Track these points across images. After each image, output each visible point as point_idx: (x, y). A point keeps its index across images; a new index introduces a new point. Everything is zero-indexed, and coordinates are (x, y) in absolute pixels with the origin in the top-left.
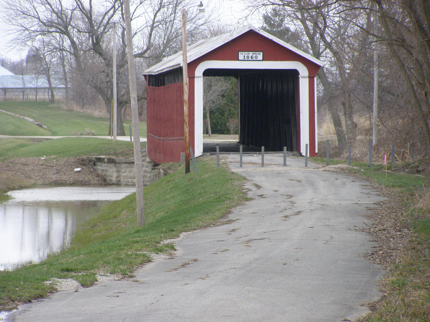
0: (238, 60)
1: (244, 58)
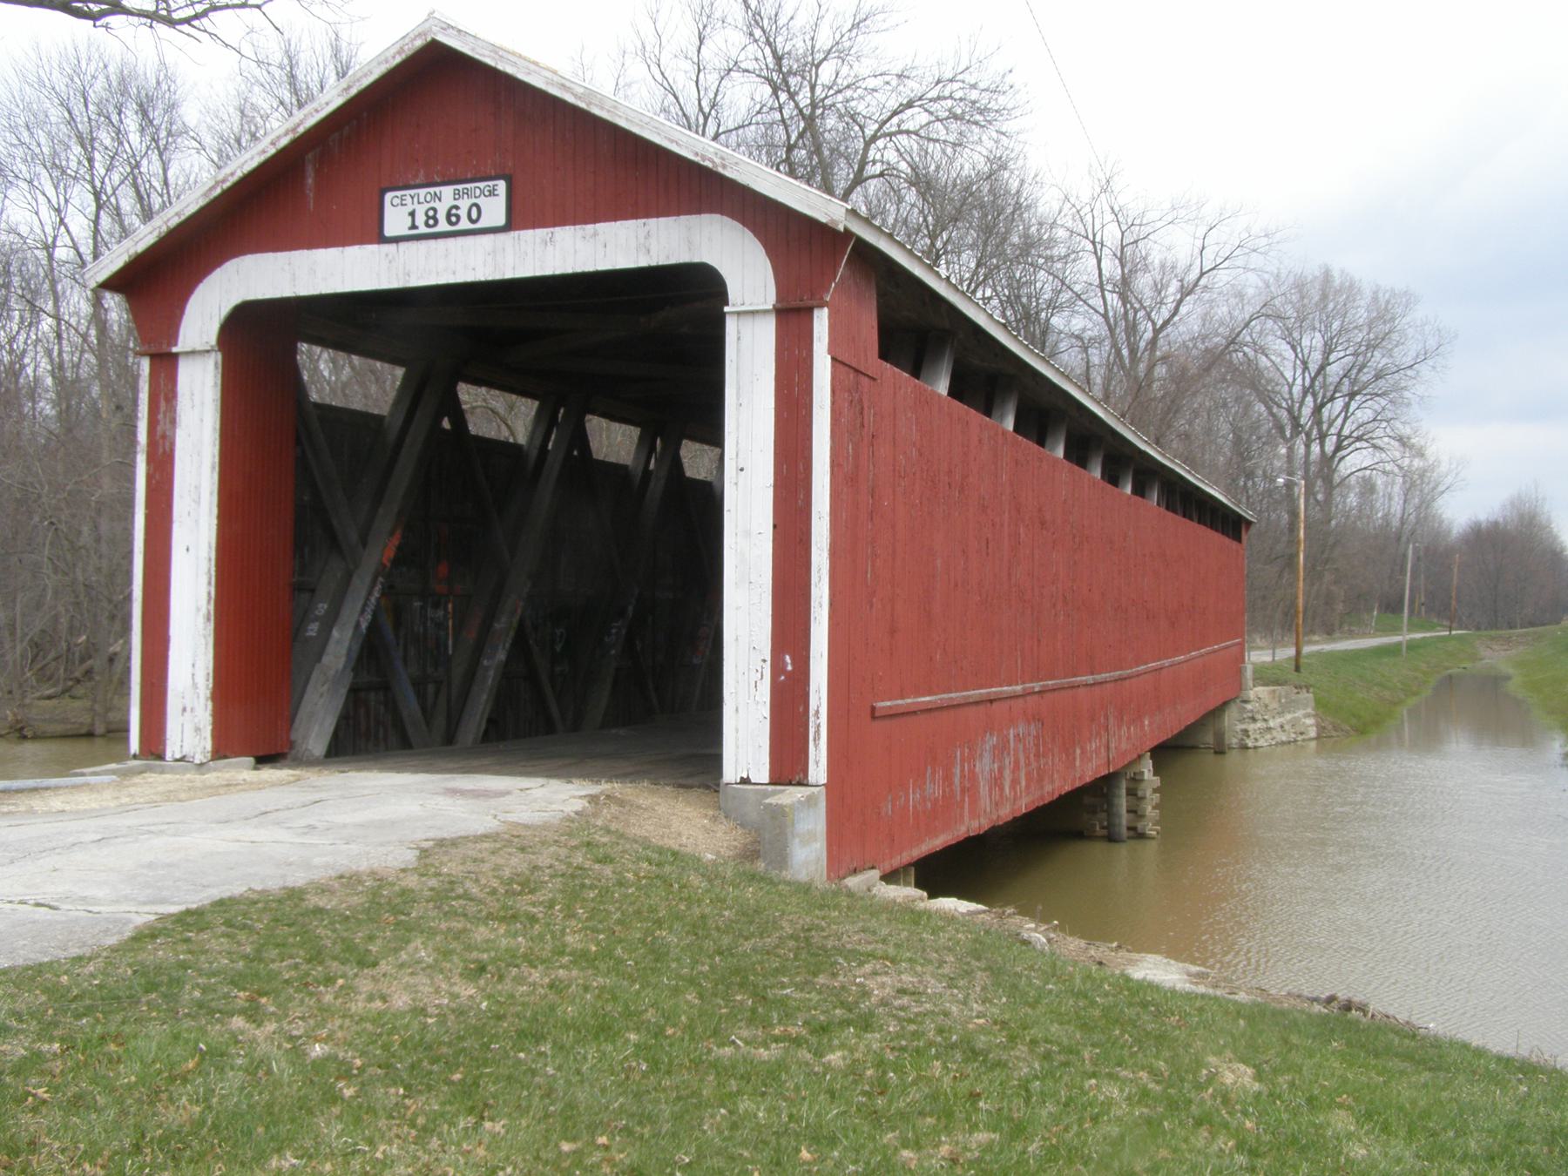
0: (381, 239)
1: (414, 227)
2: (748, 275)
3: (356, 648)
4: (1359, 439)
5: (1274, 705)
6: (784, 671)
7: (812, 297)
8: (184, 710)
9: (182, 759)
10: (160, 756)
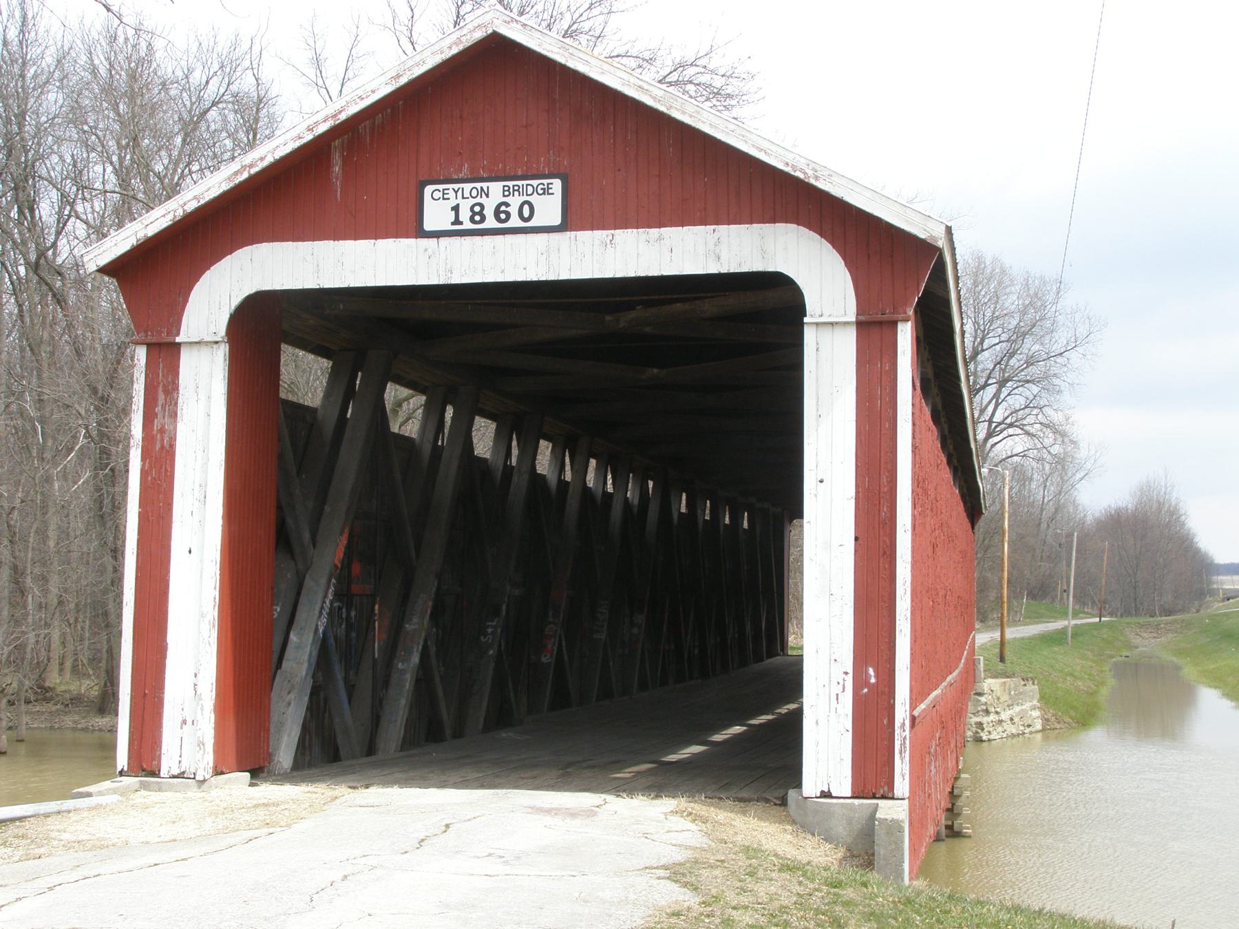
0: (419, 232)
1: (457, 222)
2: (826, 285)
3: (315, 653)
4: (1011, 425)
5: (1005, 698)
6: (867, 684)
7: (895, 311)
8: (184, 722)
9: (181, 775)
10: (155, 773)
